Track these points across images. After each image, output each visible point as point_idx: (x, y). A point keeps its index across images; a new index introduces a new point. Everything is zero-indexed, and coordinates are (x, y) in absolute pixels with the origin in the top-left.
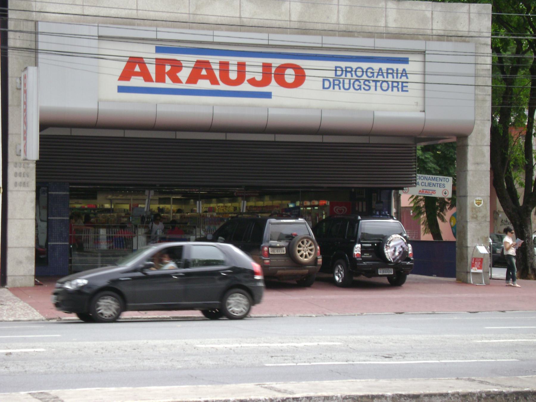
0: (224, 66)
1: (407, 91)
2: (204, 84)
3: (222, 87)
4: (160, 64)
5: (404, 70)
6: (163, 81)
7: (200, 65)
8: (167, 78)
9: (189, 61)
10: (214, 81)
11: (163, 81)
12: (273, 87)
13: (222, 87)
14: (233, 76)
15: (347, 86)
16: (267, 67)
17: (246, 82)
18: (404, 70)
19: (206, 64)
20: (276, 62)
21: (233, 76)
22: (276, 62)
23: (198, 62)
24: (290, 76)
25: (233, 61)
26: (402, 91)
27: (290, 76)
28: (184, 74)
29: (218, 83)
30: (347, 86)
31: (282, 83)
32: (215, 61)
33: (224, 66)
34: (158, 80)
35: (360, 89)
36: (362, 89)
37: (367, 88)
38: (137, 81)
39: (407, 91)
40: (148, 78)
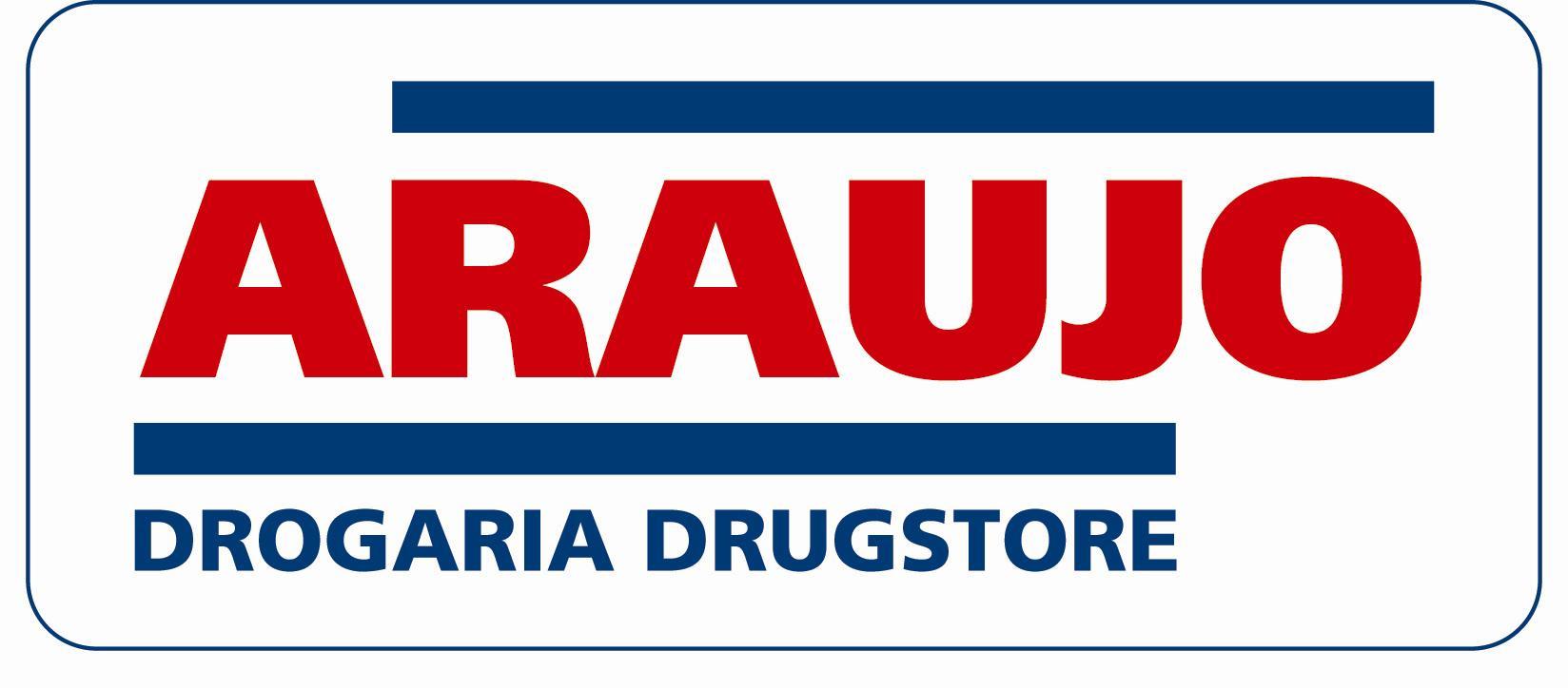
0: (886, 217)
1: (1170, 565)
2: (715, 378)
3: (863, 390)
4: (426, 215)
5: (581, 519)
6: (451, 361)
7: (684, 212)
8: (488, 333)
9: (617, 184)
10: (791, 346)
11: (451, 361)
12: (1196, 379)
13: (863, 390)
14: (948, 297)
15: (800, 548)
16: (1142, 215)
17: (1049, 344)
18: (581, 519)
19: (750, 213)
21: (948, 297)
24: (1311, 279)
25: (948, 168)
26: (1142, 562)
27: (1311, 279)
28: (597, 290)
29: (821, 364)
30: (800, 548)
31: (1261, 339)
32: (812, 184)
33: (886, 217)
35: (884, 562)
36: (898, 560)
37: (923, 553)
38: (260, 378)
39: (1170, 565)
40: (334, 348)
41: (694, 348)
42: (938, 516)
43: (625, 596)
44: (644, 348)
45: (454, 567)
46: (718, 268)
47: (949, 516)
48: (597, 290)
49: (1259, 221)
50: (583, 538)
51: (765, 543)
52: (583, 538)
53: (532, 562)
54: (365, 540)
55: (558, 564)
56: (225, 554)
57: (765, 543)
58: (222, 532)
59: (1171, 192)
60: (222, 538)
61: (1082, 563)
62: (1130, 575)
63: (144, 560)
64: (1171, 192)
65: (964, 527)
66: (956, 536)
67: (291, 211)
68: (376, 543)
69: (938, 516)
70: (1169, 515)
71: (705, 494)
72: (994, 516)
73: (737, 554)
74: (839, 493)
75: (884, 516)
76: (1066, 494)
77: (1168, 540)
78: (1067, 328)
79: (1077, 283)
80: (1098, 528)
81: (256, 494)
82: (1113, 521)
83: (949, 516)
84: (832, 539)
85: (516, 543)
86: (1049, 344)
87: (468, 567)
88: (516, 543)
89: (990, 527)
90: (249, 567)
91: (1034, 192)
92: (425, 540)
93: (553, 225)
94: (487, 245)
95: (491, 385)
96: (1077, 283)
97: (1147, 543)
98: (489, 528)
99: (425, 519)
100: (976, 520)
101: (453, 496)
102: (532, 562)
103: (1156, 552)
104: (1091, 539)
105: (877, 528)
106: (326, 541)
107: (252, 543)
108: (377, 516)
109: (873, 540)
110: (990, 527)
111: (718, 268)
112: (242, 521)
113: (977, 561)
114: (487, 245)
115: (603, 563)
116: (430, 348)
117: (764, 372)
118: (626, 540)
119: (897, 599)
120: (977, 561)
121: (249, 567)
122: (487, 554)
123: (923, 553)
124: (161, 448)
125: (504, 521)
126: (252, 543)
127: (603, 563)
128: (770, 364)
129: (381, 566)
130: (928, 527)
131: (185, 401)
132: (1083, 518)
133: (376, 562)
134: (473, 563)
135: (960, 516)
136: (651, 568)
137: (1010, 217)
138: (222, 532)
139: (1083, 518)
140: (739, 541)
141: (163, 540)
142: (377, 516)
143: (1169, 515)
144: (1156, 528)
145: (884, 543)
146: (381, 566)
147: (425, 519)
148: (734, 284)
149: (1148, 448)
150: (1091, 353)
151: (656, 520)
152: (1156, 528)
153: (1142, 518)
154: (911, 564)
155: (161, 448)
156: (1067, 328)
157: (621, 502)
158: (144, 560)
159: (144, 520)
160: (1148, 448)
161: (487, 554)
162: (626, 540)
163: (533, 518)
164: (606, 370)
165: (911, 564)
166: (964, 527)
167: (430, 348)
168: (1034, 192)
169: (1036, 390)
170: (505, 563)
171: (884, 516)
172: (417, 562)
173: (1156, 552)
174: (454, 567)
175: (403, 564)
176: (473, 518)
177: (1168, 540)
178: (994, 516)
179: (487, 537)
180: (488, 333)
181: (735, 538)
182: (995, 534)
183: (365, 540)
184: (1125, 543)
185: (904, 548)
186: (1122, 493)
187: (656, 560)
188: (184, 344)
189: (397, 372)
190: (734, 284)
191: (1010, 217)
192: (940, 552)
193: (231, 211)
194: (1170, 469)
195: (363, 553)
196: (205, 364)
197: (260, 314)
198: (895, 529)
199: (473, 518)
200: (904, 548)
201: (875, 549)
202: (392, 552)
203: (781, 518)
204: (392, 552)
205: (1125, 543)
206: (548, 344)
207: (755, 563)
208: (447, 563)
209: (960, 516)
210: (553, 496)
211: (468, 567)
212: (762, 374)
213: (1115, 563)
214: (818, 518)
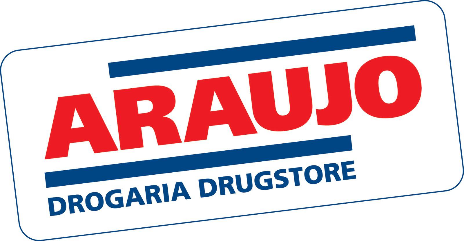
0: (261, 84)
1: (354, 177)
2: (221, 138)
3: (264, 137)
4: (125, 100)
5: (179, 185)
6: (139, 143)
7: (205, 89)
8: (148, 133)
9: (183, 84)
10: (242, 127)
11: (139, 143)
12: (358, 123)
13: (264, 137)
14: (283, 106)
15: (245, 185)
16: (336, 74)
17: (314, 117)
18: (179, 185)
19: (224, 87)
20: (355, 59)
21: (283, 106)
22: (355, 59)
23: (201, 84)
24: (388, 87)
25: (278, 68)
26: (346, 177)
27: (388, 87)
28: (180, 116)
30: (245, 185)
33: (261, 84)
34: (125, 146)
35: (270, 187)
36: (274, 186)
37: (281, 182)
38: (81, 155)
39: (354, 177)
40: (102, 143)
41: (213, 130)
42: (284, 171)
43: (195, 206)
44: (197, 131)
45: (144, 204)
46: (216, 104)
47: (287, 171)
48: (180, 116)
49: (371, 71)
50: (181, 191)
51: (234, 185)
52: (181, 191)
53: (167, 199)
54: (117, 199)
55: (174, 199)
56: (76, 208)
57: (234, 185)
58: (151, 192)
59: (344, 65)
60: (75, 204)
61: (328, 180)
62: (342, 182)
63: (53, 213)
64: (344, 65)
65: (292, 173)
66: (290, 176)
67: (84, 104)
68: (120, 199)
69: (284, 171)
70: (352, 163)
71: (214, 173)
72: (301, 169)
73: (76, 208)
74: (254, 168)
75: (268, 173)
76: (321, 160)
77: (352, 170)
78: (318, 111)
79: (320, 98)
80: (332, 169)
81: (83, 189)
82: (336, 166)
83: (287, 171)
84: (254, 182)
85: (161, 194)
86: (314, 117)
87: (148, 203)
88: (161, 194)
89: (300, 172)
90: (235, 193)
91: (305, 70)
92: (134, 197)
93: (164, 98)
94: (145, 107)
95: (151, 148)
96: (320, 98)
97: (346, 171)
98: (152, 191)
99: (134, 190)
100: (295, 171)
101: (141, 183)
102: (167, 199)
103: (349, 174)
104: (330, 172)
105: (117, 195)
106: (105, 200)
107: (83, 204)
108: (119, 191)
109: (266, 181)
110: (300, 172)
111: (216, 104)
112: (80, 197)
113: (297, 183)
114: (145, 107)
115: (187, 197)
116: (132, 140)
117: (235, 134)
118: (193, 189)
119: (275, 197)
120: (297, 183)
121: (235, 193)
122: (153, 199)
123: (281, 182)
124: (54, 179)
125: (157, 188)
126: (83, 204)
127: (187, 197)
128: (236, 132)
129: (122, 206)
130: (282, 175)
131: (59, 165)
132: (221, 179)
133: (121, 205)
134: (149, 202)
135: (290, 170)
136: (202, 196)
137: (298, 80)
138: (151, 192)
139: (327, 166)
140: (227, 186)
141: (57, 206)
142: (119, 191)
143: (352, 163)
144: (349, 167)
145: (269, 181)
146: (122, 206)
147: (134, 190)
148: (211, 110)
149: (343, 144)
150: (327, 117)
151: (202, 182)
152: (349, 167)
153: (344, 164)
154: (278, 186)
155: (54, 179)
156: (318, 111)
157: (190, 178)
158: (53, 213)
159: (51, 201)
160: (343, 144)
161: (153, 199)
162: (193, 189)
163: (165, 186)
164: (187, 140)
165: (278, 186)
166: (292, 173)
167: (132, 140)
168: (305, 70)
169: (311, 130)
170: (159, 200)
171: (268, 173)
172: (178, 198)
173: (349, 174)
174: (144, 204)
175: (129, 204)
176: (148, 188)
177: (352, 170)
178: (301, 169)
179: (152, 193)
180: (148, 133)
181: (225, 185)
182: (301, 174)
183: (117, 199)
184: (340, 172)
185: (275, 182)
186: (337, 158)
187: (203, 194)
188: (57, 148)
189: (122, 148)
190: (211, 110)
191: (298, 80)
192: (286, 182)
193: (66, 106)
194: (351, 149)
195: (117, 203)
196: (64, 153)
197: (79, 136)
198: (272, 176)
199: (148, 188)
200: (275, 182)
201: (118, 202)
202: (125, 202)
203: (238, 177)
204: (125, 202)
205: (340, 172)
206: (167, 134)
207: (232, 191)
208: (142, 203)
209: (290, 170)
210: (170, 179)
211: (148, 203)
212: (235, 134)
213: (338, 178)
214: (249, 176)
